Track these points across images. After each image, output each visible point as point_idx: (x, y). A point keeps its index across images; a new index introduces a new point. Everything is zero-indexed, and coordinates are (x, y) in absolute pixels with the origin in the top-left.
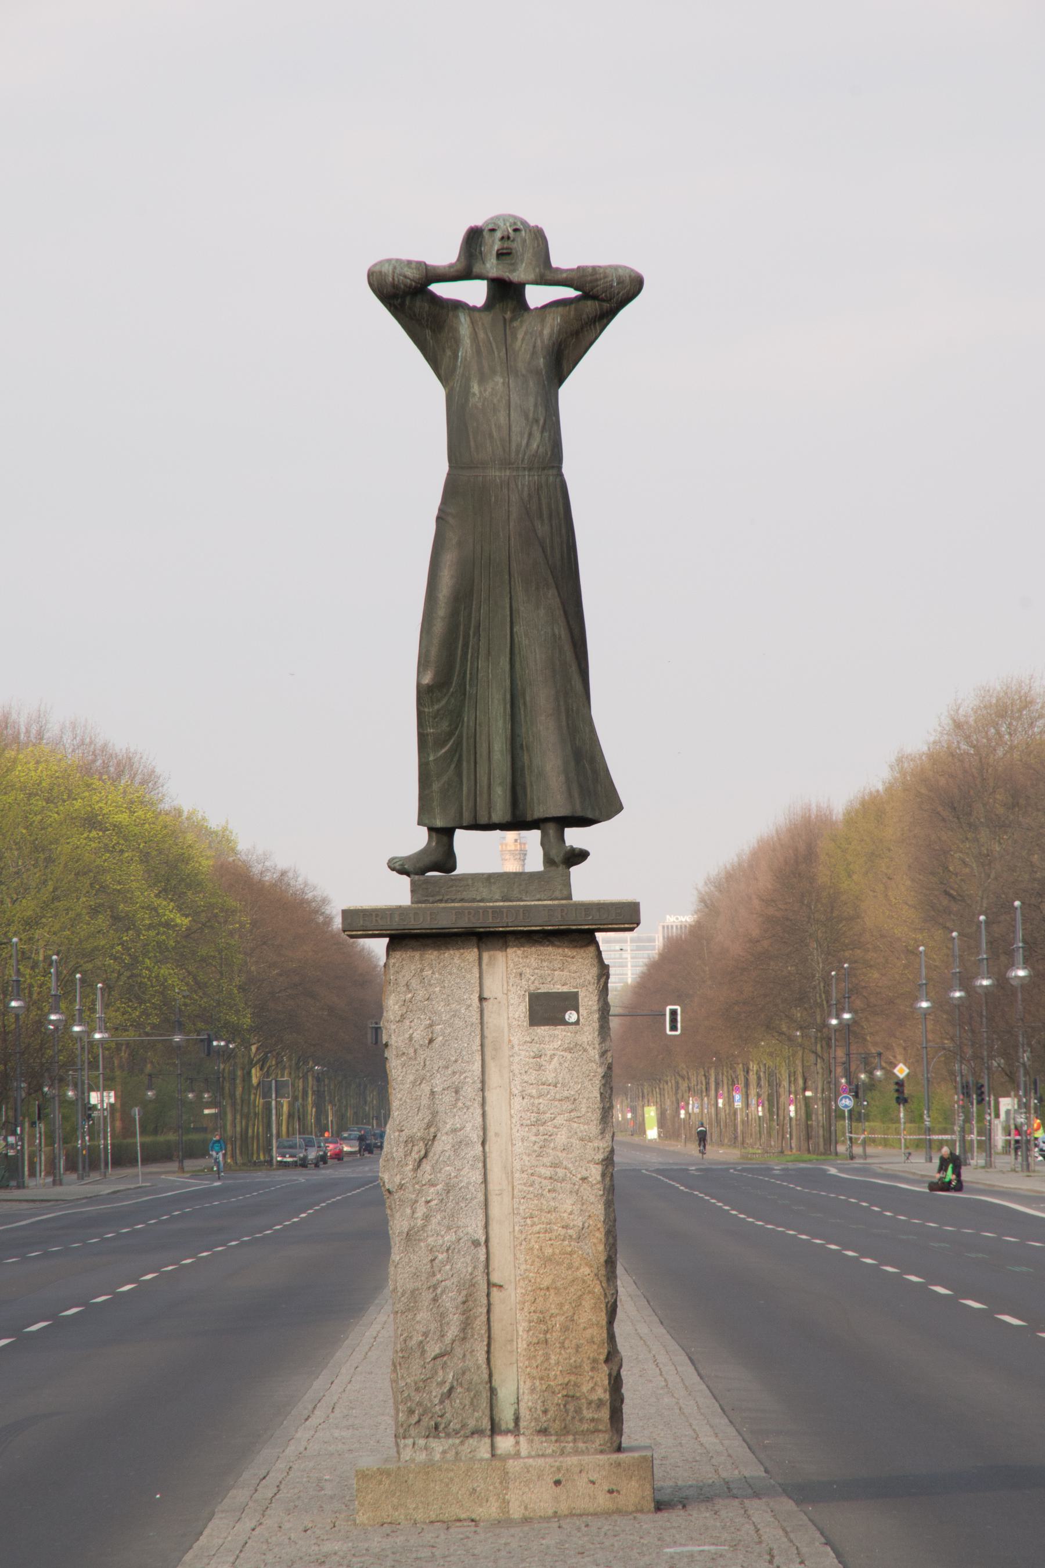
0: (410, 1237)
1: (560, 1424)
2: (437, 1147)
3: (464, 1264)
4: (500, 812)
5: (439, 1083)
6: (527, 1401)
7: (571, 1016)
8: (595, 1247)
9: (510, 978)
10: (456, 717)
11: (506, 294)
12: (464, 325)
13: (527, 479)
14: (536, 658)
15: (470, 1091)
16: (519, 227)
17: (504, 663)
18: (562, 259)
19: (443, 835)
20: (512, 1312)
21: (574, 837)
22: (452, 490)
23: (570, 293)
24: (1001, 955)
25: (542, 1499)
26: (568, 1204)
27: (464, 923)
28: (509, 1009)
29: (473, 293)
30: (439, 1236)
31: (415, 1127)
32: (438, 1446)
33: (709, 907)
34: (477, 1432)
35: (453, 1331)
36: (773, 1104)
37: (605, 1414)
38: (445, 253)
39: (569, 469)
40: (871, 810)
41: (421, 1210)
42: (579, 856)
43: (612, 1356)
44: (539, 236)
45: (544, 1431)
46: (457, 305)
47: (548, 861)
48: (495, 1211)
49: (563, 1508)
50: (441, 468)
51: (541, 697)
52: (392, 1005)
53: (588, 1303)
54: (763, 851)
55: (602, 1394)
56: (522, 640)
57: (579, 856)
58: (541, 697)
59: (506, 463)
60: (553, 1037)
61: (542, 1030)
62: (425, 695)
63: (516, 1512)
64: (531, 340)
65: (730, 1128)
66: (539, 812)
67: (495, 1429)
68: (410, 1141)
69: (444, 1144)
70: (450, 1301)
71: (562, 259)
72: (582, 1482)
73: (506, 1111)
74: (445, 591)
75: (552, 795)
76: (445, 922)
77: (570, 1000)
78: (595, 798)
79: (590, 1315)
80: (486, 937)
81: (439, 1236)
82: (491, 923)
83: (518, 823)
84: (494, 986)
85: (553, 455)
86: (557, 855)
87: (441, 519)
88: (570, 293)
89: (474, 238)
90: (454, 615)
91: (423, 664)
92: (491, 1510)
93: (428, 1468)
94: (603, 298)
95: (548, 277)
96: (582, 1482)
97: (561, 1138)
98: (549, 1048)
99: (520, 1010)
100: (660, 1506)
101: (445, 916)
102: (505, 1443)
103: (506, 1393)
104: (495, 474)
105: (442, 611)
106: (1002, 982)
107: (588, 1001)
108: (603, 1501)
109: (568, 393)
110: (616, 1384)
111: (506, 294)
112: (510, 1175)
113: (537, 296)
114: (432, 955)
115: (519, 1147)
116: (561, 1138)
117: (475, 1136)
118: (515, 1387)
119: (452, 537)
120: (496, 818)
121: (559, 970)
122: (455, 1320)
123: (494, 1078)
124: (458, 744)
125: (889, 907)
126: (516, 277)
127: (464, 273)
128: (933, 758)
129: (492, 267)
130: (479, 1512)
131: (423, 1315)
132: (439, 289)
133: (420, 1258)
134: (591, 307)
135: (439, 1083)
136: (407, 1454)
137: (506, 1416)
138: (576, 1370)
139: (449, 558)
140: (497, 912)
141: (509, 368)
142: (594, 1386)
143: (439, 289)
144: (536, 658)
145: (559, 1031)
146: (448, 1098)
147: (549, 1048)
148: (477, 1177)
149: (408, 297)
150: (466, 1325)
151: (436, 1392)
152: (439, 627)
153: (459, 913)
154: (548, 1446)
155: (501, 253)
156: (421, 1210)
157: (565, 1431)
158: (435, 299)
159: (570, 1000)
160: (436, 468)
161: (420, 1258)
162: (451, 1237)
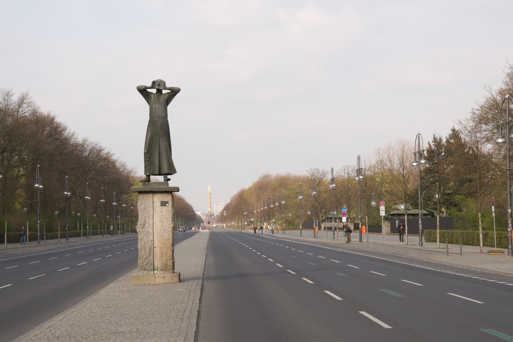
0: (141, 239)
1: (164, 269)
2: (146, 225)
3: (149, 244)
4: (157, 173)
5: (146, 215)
6: (159, 265)
7: (167, 205)
8: (171, 241)
9: (158, 199)
10: (150, 158)
11: (159, 91)
12: (152, 96)
13: (161, 120)
14: (163, 148)
15: (151, 216)
16: (161, 81)
17: (158, 149)
18: (168, 86)
19: (148, 176)
20: (157, 251)
21: (169, 177)
22: (150, 122)
23: (169, 91)
24: (264, 206)
25: (161, 281)
26: (166, 234)
27: (150, 190)
28: (157, 204)
29: (154, 91)
30: (146, 239)
31: (142, 222)
32: (145, 272)
33: (232, 200)
34: (151, 270)
35: (148, 254)
36: (238, 223)
37: (172, 267)
38: (149, 84)
39: (169, 119)
40: (250, 188)
41: (143, 235)
42: (169, 180)
43: (173, 258)
44: (164, 82)
45: (162, 270)
46: (151, 93)
47: (165, 180)
48: (155, 235)
49: (164, 282)
50: (149, 118)
51: (164, 155)
52: (139, 203)
53: (169, 250)
54: (238, 193)
55: (171, 264)
56: (161, 145)
57: (169, 180)
58: (164, 155)
59: (158, 117)
60: (164, 208)
61: (163, 207)
62: (145, 154)
63: (157, 283)
64: (163, 99)
65: (232, 227)
66: (163, 173)
67: (154, 270)
68: (141, 224)
69: (147, 225)
70: (147, 250)
71: (168, 86)
72: (167, 278)
73: (157, 220)
74: (149, 137)
75: (165, 170)
76: (147, 190)
77: (167, 202)
78: (172, 171)
79: (170, 252)
80: (154, 192)
81: (146, 239)
82: (154, 190)
83: (160, 174)
84: (155, 200)
85: (166, 116)
86: (166, 179)
87: (148, 126)
88: (169, 91)
89: (154, 82)
90: (150, 141)
91: (145, 149)
92: (153, 282)
93: (143, 276)
94: (174, 92)
95: (166, 88)
96: (167, 278)
97: (165, 224)
98: (164, 210)
99: (159, 204)
100: (180, 281)
101: (147, 189)
102: (156, 272)
103: (156, 264)
104: (156, 119)
105: (148, 141)
106: (264, 209)
107: (170, 202)
108: (171, 281)
109: (169, 107)
110: (174, 263)
111: (159, 91)
112: (157, 230)
113: (164, 92)
114: (145, 195)
115: (159, 226)
116: (165, 224)
117: (152, 224)
118: (157, 263)
119: (150, 129)
120: (157, 173)
121: (167, 198)
122: (148, 253)
123: (155, 215)
124: (150, 162)
125: (253, 200)
126: (160, 88)
127: (152, 87)
128: (257, 182)
129: (157, 87)
130: (151, 283)
131: (143, 252)
132: (148, 90)
133: (143, 243)
134: (172, 93)
135: (146, 215)
136: (140, 273)
137: (156, 268)
138: (167, 260)
139: (149, 132)
140: (155, 188)
141: (159, 103)
142: (170, 263)
143: (148, 90)
144: (163, 148)
145: (165, 207)
146: (147, 218)
147: (164, 210)
148: (152, 230)
149: (143, 91)
150: (150, 253)
151: (145, 264)
152: (147, 143)
153: (149, 188)
154: (163, 272)
155: (158, 85)
156: (143, 235)
157: (165, 270)
158: (147, 92)
159: (167, 202)
160: (148, 118)
161: (143, 243)
162: (147, 240)
